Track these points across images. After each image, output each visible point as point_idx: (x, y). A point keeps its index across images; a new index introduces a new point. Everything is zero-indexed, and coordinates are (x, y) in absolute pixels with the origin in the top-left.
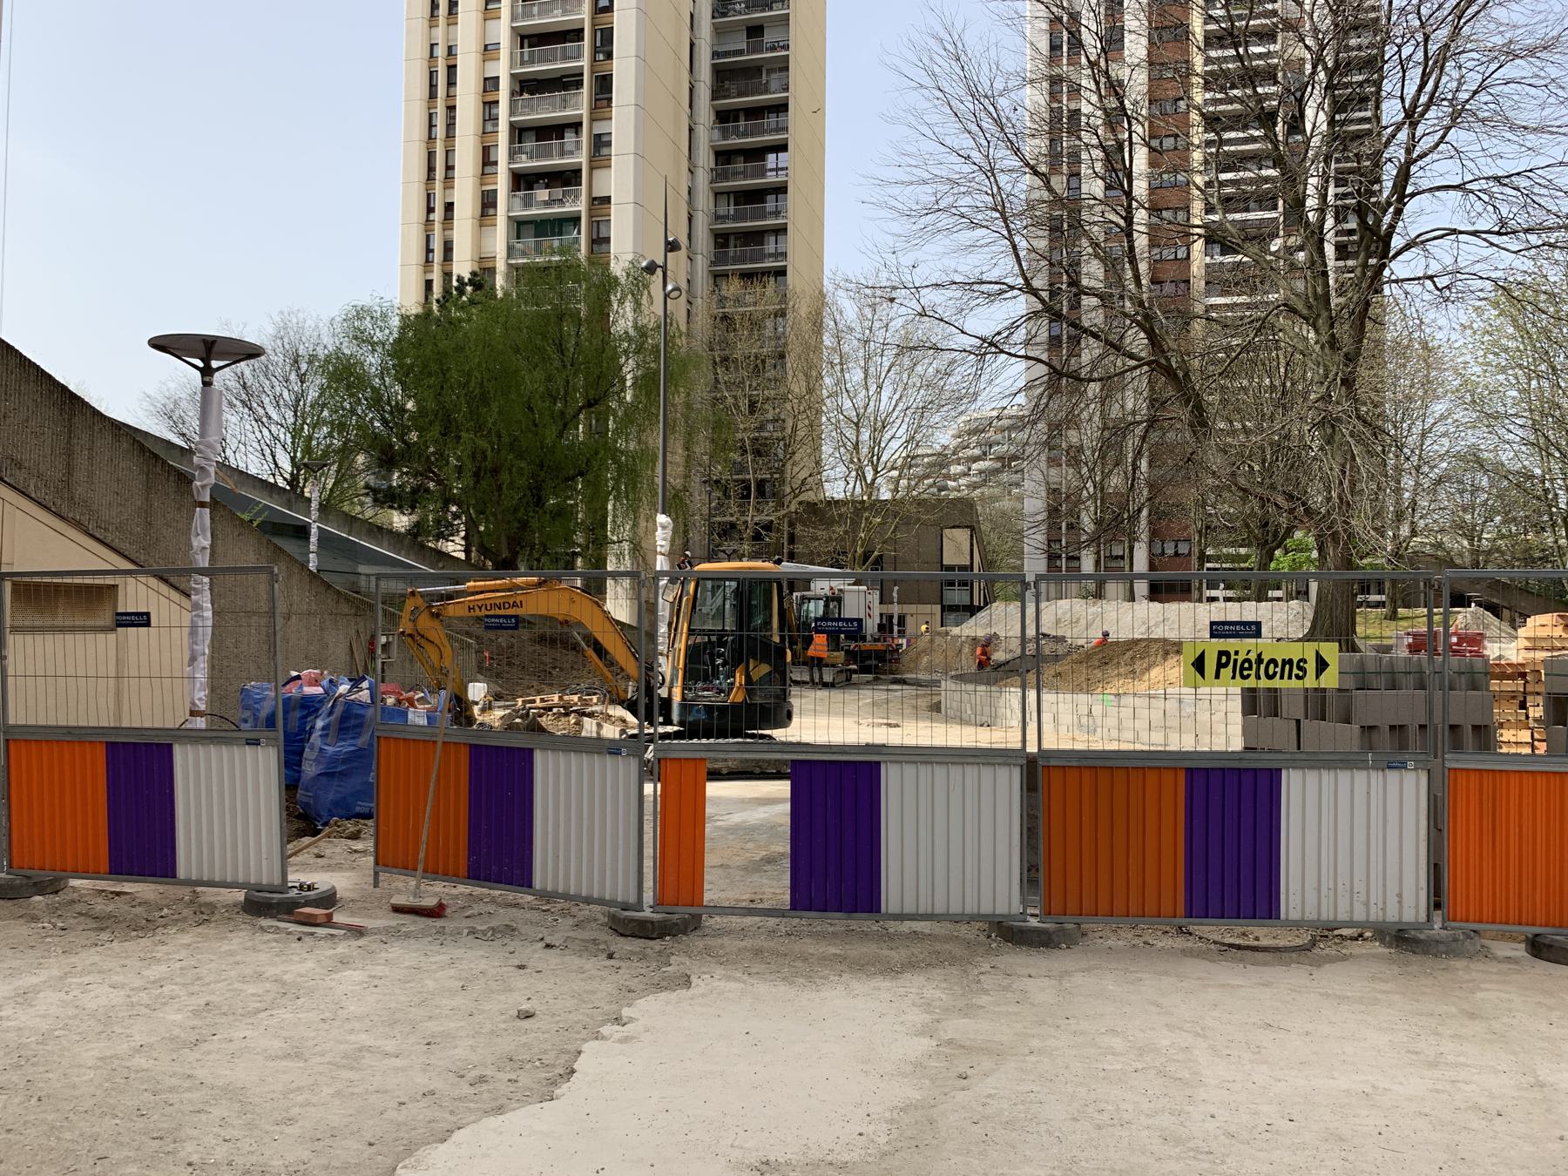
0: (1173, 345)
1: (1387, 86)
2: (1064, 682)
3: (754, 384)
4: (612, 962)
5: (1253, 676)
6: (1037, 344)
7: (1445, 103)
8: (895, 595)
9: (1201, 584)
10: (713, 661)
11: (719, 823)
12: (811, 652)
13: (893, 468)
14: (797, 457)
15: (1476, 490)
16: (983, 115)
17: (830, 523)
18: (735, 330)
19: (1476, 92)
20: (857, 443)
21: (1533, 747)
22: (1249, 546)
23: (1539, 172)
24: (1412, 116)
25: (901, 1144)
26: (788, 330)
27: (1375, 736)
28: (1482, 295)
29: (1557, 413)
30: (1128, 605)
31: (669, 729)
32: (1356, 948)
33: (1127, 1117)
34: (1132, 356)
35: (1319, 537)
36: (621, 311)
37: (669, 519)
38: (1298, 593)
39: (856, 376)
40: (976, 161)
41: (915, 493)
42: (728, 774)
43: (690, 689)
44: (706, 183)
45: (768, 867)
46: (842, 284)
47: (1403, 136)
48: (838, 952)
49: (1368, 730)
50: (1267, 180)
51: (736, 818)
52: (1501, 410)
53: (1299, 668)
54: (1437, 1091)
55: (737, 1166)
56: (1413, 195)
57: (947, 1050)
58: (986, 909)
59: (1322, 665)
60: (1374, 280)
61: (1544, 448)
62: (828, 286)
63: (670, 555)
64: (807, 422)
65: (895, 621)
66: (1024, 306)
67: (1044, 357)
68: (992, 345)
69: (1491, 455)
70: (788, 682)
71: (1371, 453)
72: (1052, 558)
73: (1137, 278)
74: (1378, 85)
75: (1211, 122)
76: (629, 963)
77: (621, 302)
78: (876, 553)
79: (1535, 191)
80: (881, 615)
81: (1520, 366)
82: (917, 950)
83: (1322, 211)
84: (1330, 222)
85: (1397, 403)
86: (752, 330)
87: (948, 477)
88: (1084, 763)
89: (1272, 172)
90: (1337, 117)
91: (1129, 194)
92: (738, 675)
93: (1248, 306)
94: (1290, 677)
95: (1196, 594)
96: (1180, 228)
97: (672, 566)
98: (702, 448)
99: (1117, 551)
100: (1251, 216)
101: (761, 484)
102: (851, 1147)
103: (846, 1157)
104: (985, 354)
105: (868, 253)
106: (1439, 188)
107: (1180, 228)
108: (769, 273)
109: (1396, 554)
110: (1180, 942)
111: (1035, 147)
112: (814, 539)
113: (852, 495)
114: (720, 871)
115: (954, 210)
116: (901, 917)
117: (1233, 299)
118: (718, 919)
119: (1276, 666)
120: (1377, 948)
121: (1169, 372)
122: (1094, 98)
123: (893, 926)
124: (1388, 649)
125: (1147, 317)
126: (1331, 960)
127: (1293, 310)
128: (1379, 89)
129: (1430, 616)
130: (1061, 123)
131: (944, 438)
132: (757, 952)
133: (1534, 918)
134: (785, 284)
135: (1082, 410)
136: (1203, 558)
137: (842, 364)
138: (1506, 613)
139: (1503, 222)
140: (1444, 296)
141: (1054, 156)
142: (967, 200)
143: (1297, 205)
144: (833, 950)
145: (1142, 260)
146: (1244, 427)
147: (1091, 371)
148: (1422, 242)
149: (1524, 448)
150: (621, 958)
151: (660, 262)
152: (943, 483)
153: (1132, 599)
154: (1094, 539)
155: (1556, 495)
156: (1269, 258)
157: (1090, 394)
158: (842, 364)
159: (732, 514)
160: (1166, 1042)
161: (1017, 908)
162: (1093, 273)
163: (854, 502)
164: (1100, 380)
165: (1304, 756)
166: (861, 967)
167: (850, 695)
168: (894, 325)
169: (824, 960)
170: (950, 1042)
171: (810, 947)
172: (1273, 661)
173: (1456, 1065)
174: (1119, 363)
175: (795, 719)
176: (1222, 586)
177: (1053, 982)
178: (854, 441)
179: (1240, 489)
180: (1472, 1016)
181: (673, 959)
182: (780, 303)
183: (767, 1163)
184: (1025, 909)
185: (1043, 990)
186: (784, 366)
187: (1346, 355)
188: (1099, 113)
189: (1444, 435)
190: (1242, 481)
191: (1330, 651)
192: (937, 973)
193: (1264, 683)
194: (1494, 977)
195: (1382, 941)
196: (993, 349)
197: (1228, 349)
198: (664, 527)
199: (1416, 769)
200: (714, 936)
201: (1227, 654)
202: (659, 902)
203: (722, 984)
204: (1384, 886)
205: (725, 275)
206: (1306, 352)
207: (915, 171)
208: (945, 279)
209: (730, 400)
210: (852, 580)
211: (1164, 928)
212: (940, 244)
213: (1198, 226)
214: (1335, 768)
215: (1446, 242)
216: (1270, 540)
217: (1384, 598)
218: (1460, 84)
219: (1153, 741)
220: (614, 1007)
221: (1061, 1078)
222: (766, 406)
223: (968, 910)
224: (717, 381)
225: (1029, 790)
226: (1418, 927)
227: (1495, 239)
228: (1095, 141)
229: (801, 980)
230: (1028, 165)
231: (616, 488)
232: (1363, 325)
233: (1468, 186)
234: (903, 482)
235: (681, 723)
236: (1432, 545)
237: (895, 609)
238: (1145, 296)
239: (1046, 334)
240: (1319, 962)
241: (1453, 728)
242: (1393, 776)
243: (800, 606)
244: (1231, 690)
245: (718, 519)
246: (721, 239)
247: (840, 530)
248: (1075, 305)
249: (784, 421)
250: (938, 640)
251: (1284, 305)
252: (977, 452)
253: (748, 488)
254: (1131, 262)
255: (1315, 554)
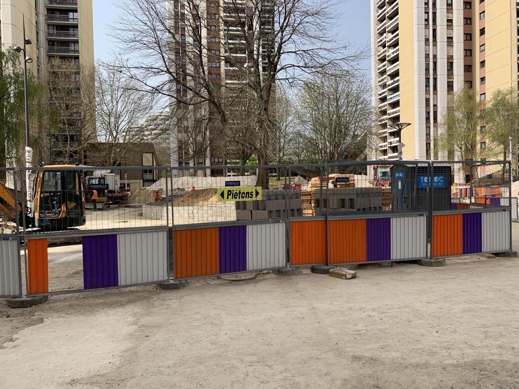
0: (216, 95)
1: (276, 19)
2: (183, 204)
3: (68, 99)
4: (9, 319)
5: (238, 198)
6: (172, 91)
7: (291, 26)
8: (126, 177)
9: (226, 171)
10: (52, 203)
11: (56, 262)
12: (93, 198)
13: (123, 132)
14: (86, 127)
15: (300, 142)
16: (151, 9)
17: (100, 151)
18: (58, 78)
19: (299, 24)
20: (110, 122)
21: (313, 214)
22: (239, 159)
23: (315, 50)
24: (282, 29)
25: (125, 363)
26: (81, 79)
27: (272, 214)
28: (301, 86)
29: (319, 121)
30: (204, 178)
31: (35, 229)
32: (268, 276)
33: (200, 339)
34: (203, 97)
35: (258, 156)
36: (7, 66)
37: (31, 149)
38: (253, 173)
39: (108, 98)
40: (149, 25)
41: (132, 141)
42: (60, 244)
43: (43, 214)
44: (44, 20)
45: (76, 275)
46: (101, 64)
47: (280, 35)
48: (102, 301)
49: (270, 212)
50: (243, 44)
51: (63, 259)
52: (306, 120)
53: (251, 195)
54: (288, 314)
55: (61, 384)
56: (282, 53)
57: (142, 329)
58: (156, 279)
59: (257, 193)
60: (273, 78)
61: (316, 131)
62: (96, 65)
63: (33, 162)
64: (89, 114)
65: (126, 185)
66: (168, 78)
67: (175, 95)
68: (156, 90)
69: (303, 133)
70: (83, 208)
71: (273, 132)
72: (180, 163)
73: (204, 71)
74: (273, 18)
75: (226, 23)
76: (17, 318)
77: (6, 62)
78: (118, 162)
79: (314, 55)
80: (121, 184)
81: (310, 107)
82: (132, 296)
83: (258, 55)
84: (260, 59)
85: (279, 116)
86: (66, 78)
87: (144, 135)
88: (187, 228)
89: (244, 42)
90: (262, 27)
91: (200, 43)
92: (63, 207)
93: (238, 84)
94: (248, 198)
95: (224, 175)
96: (217, 57)
97: (33, 166)
98: (46, 121)
99: (201, 161)
100: (238, 55)
101: (72, 137)
102: (106, 368)
103: (104, 372)
104: (154, 93)
105: (111, 54)
106: (289, 52)
107: (217, 57)
108: (72, 58)
109: (279, 162)
110: (218, 282)
111: (169, 23)
112: (94, 157)
113: (108, 141)
114: (56, 279)
115: (141, 42)
116: (126, 286)
117: (234, 82)
118: (55, 296)
119: (244, 194)
120: (273, 275)
121: (214, 103)
122: (189, 9)
123: (123, 290)
124: (277, 189)
125: (207, 85)
126: (261, 281)
127: (250, 86)
128: (273, 20)
129: (286, 179)
130: (179, 17)
131: (142, 122)
132: (71, 306)
133: (362, 260)
134: (79, 62)
135: (188, 114)
136: (226, 163)
137: (102, 93)
138: (307, 178)
139: (306, 64)
140: (291, 85)
141: (176, 28)
142: (146, 39)
143: (251, 52)
144: (470, 260)
145: (205, 66)
146: (237, 122)
147: (190, 101)
148: (285, 68)
149: (311, 131)
150: (13, 317)
151: (22, 48)
152: (142, 137)
153: (205, 176)
154: (193, 157)
155: (319, 144)
156: (244, 69)
157: (190, 108)
158: (102, 93)
159: (60, 147)
160: (213, 313)
161: (166, 278)
162: (190, 69)
163: (109, 143)
164: (193, 104)
165: (252, 221)
166: (111, 305)
167: (110, 212)
168: (123, 80)
169: (97, 305)
170: (143, 326)
171: (92, 301)
172: (244, 193)
173: (293, 306)
174: (199, 99)
175: (87, 222)
176: (232, 171)
177: (178, 300)
178: (108, 122)
179: (236, 141)
180: (297, 291)
181: (36, 314)
182: (77, 69)
183: (74, 380)
184: (169, 278)
185: (174, 303)
186: (79, 93)
187: (265, 101)
188: (190, 15)
189: (291, 127)
190: (237, 139)
191: (259, 189)
192: (138, 303)
193: (241, 200)
194: (303, 280)
195: (274, 273)
196: (157, 92)
197: (232, 97)
198: (29, 152)
199: (282, 222)
200: (53, 303)
201: (230, 191)
202: (29, 293)
203: (56, 319)
204: (275, 257)
205: (53, 56)
206: (254, 99)
207: (127, 26)
208: (139, 65)
209: (57, 104)
210: (109, 171)
211: (213, 278)
212: (137, 53)
213: (222, 56)
214: (261, 224)
215: (291, 68)
216: (245, 157)
217: (276, 174)
218: (295, 21)
219: (211, 220)
220: (10, 335)
221: (180, 331)
222: (73, 107)
223: (149, 281)
224: (52, 97)
225: (169, 239)
226: (283, 268)
227: (304, 69)
228: (189, 24)
229: (88, 313)
230: (167, 29)
231: (8, 136)
232: (269, 92)
233: (297, 52)
234: (127, 137)
235: (39, 227)
236: (289, 159)
237: (126, 182)
238: (206, 78)
239: (175, 88)
240: (257, 282)
241: (292, 210)
242: (276, 225)
243: (89, 181)
244: (232, 202)
245: (54, 149)
246: (51, 43)
247: (104, 153)
248: (185, 79)
249: (80, 113)
250: (142, 192)
251: (248, 84)
252: (153, 127)
253: (67, 138)
254: (201, 66)
255: (257, 161)
